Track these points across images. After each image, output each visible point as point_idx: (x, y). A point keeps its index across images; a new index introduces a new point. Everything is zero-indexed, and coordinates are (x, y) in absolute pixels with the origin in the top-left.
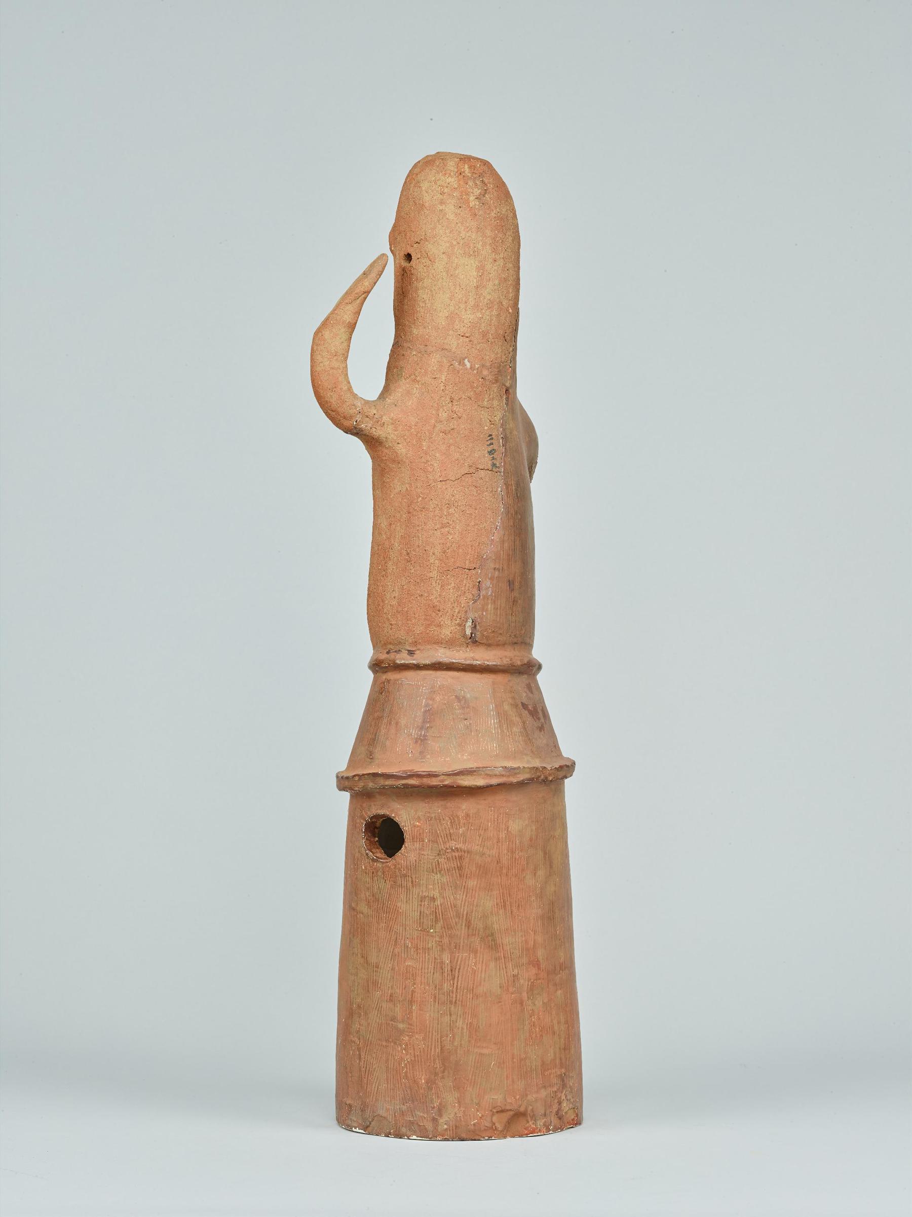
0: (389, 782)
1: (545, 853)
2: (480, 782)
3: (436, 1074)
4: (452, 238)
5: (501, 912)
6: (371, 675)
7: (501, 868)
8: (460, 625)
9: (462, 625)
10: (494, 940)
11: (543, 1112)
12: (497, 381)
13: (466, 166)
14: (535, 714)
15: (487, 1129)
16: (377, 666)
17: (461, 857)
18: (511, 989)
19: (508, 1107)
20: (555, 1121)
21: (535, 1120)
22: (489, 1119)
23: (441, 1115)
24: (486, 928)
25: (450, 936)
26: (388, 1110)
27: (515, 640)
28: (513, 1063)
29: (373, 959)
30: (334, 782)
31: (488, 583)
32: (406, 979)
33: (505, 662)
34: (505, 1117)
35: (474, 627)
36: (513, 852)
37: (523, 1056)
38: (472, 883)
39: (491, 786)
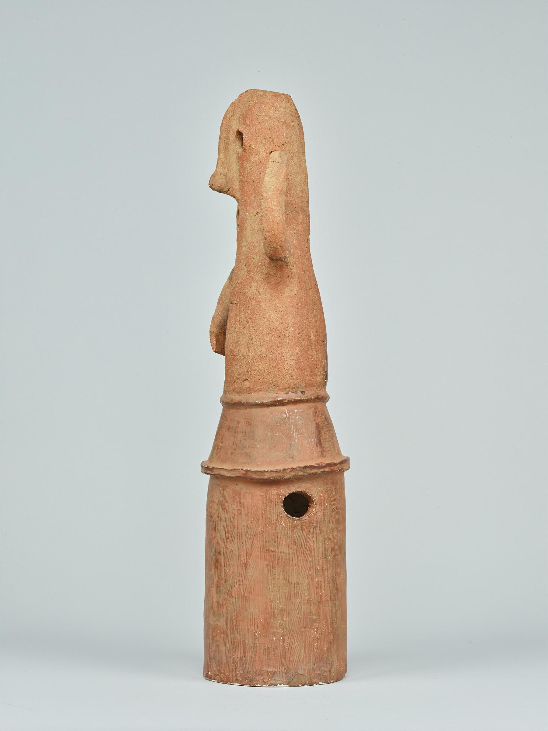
0: (314, 471)
3: (331, 643)
4: (256, 140)
23: (332, 668)
25: (336, 560)
26: (304, 670)
29: (294, 579)
30: (200, 468)
32: (317, 588)
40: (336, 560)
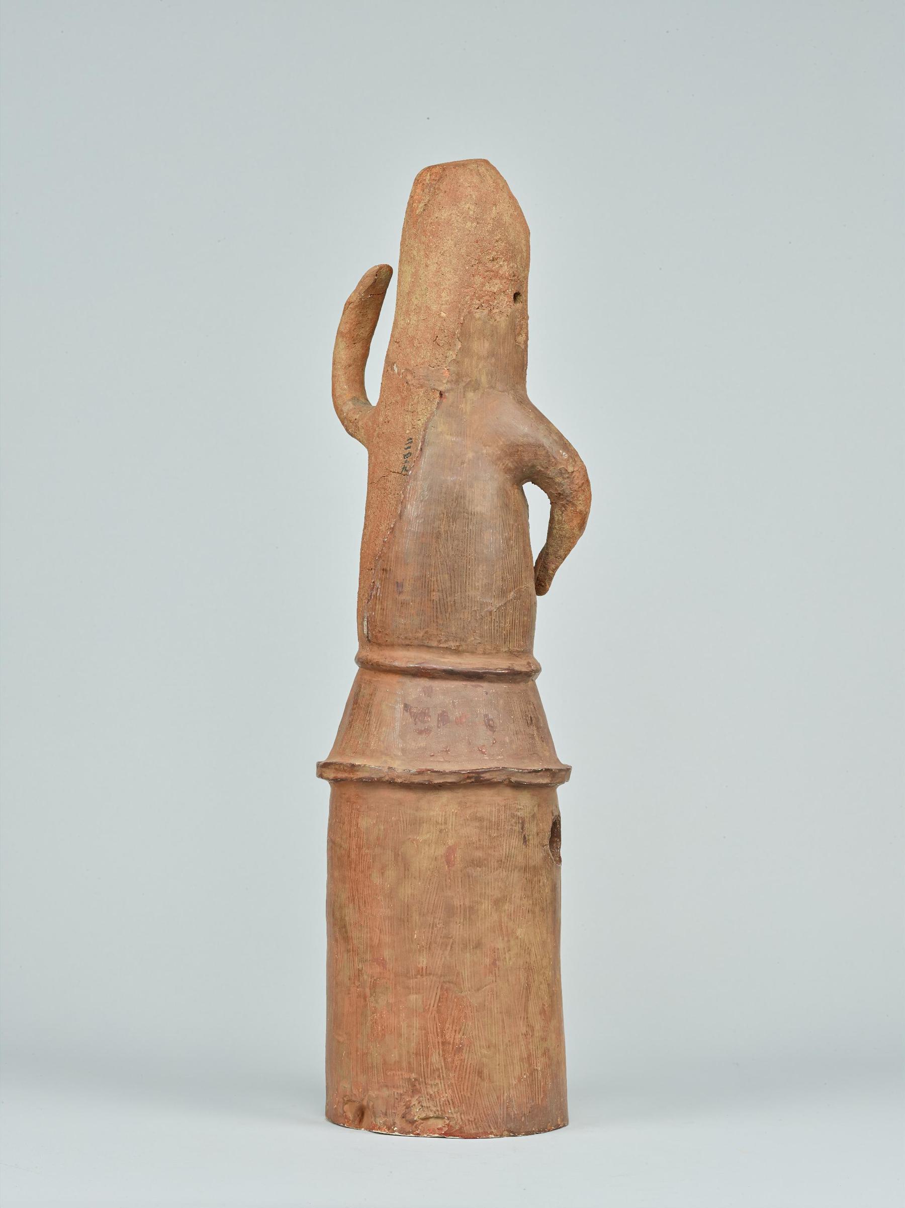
1: (396, 855)
5: (351, 905)
7: (351, 862)
11: (384, 1111)
12: (422, 387)
14: (535, 720)
18: (357, 983)
27: (408, 642)
33: (387, 662)
37: (365, 1051)
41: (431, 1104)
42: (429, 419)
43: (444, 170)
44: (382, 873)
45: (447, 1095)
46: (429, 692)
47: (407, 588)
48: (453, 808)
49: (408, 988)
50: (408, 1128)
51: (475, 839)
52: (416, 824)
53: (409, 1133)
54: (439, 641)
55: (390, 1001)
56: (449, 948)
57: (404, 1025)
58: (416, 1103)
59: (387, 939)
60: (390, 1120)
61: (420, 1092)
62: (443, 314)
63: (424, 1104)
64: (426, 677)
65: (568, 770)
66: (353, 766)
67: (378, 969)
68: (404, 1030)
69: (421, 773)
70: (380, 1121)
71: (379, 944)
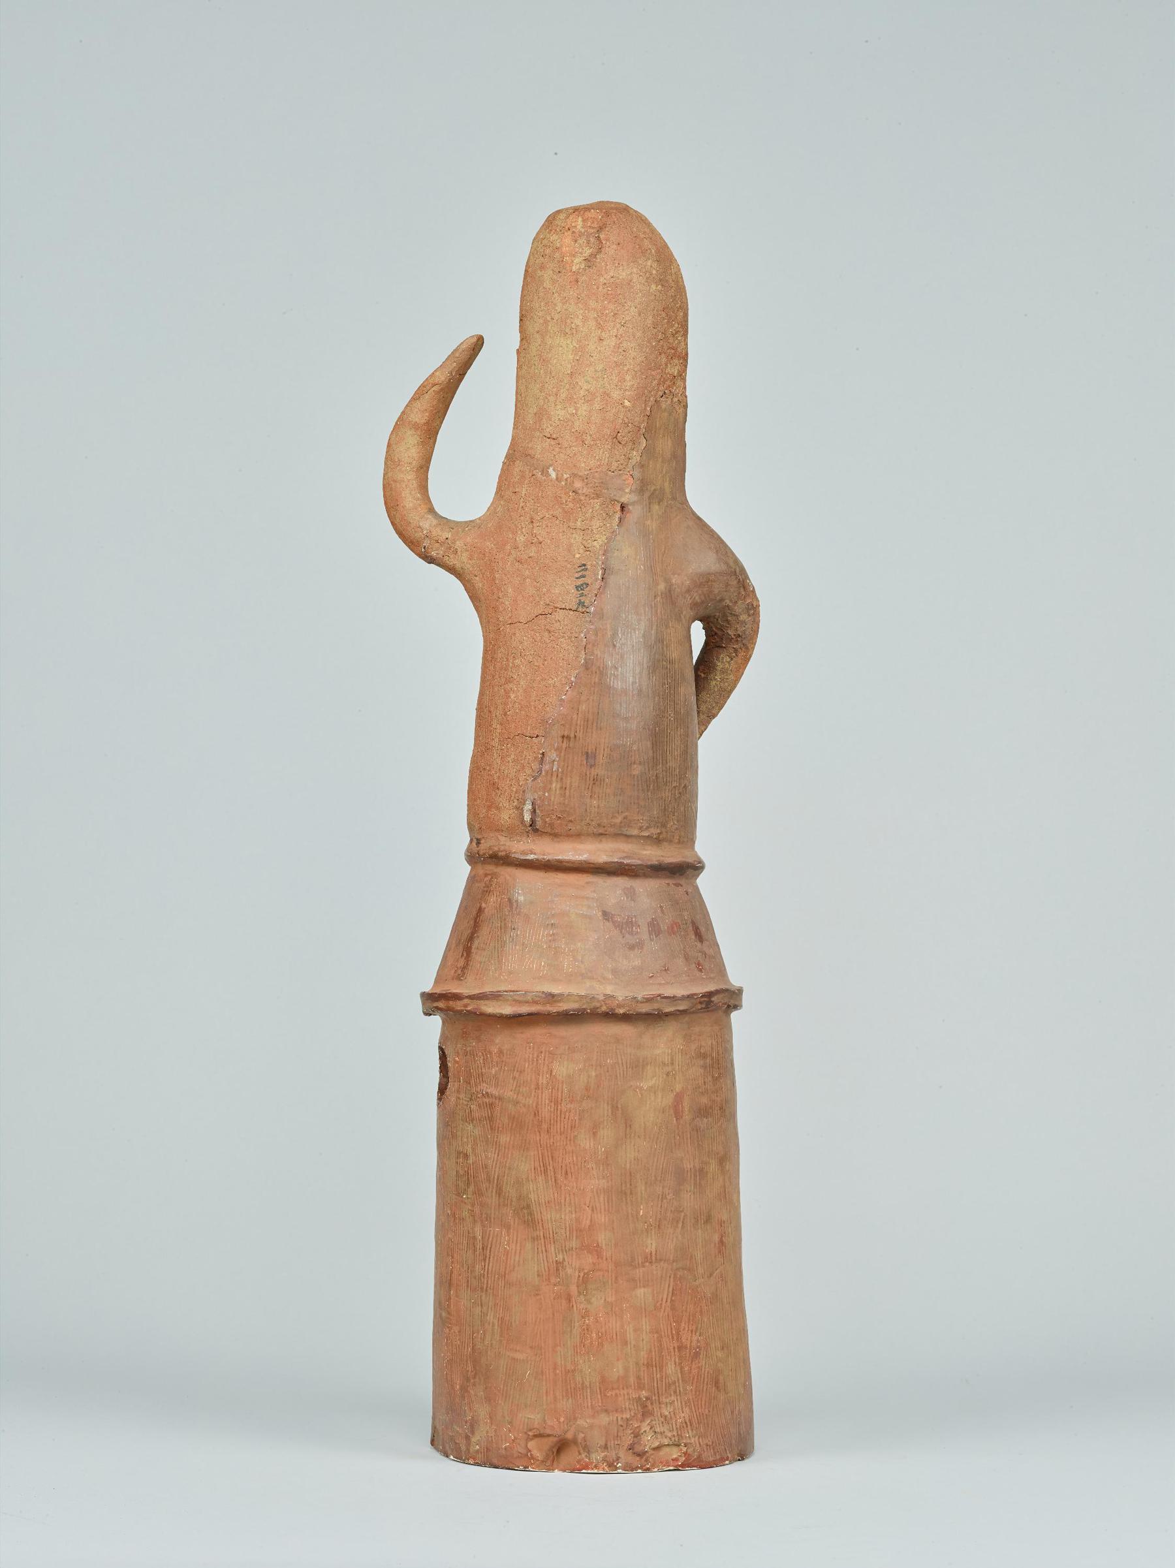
1: (615, 1108)
2: (507, 1010)
3: (468, 1380)
5: (541, 1179)
6: (468, 868)
8: (517, 808)
9: (519, 809)
10: (531, 1214)
11: (602, 1443)
12: (598, 496)
13: (580, 219)
14: (698, 929)
15: (522, 1456)
16: (473, 857)
17: (491, 1105)
19: (548, 1432)
20: (626, 1457)
21: (589, 1452)
22: (522, 1443)
23: (473, 1433)
24: (520, 1198)
25: (482, 1205)
27: (601, 831)
28: (556, 1374)
30: (745, 998)
31: (553, 755)
34: (548, 1443)
35: (534, 811)
36: (556, 1103)
37: (570, 1367)
38: (504, 1139)
39: (520, 1015)
40: (482, 1205)
41: (665, 1428)
42: (609, 540)
43: (607, 214)
44: (594, 1134)
45: (684, 1415)
46: (631, 894)
47: (601, 759)
48: (679, 1043)
49: (634, 1280)
50: (636, 1461)
51: (701, 1081)
52: (638, 1066)
53: (637, 1468)
54: (641, 828)
55: (609, 1300)
56: (680, 1225)
57: (630, 1329)
58: (648, 1429)
59: (602, 1218)
60: (612, 1455)
61: (652, 1414)
62: (627, 403)
63: (658, 1430)
64: (627, 875)
65: (739, 992)
66: (553, 996)
67: (589, 1260)
68: (631, 1335)
69: (648, 1000)
70: (597, 1456)
71: (592, 1226)
